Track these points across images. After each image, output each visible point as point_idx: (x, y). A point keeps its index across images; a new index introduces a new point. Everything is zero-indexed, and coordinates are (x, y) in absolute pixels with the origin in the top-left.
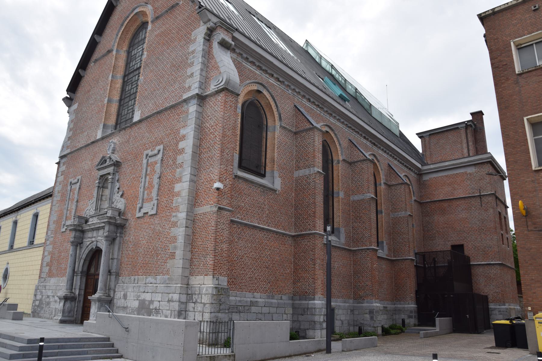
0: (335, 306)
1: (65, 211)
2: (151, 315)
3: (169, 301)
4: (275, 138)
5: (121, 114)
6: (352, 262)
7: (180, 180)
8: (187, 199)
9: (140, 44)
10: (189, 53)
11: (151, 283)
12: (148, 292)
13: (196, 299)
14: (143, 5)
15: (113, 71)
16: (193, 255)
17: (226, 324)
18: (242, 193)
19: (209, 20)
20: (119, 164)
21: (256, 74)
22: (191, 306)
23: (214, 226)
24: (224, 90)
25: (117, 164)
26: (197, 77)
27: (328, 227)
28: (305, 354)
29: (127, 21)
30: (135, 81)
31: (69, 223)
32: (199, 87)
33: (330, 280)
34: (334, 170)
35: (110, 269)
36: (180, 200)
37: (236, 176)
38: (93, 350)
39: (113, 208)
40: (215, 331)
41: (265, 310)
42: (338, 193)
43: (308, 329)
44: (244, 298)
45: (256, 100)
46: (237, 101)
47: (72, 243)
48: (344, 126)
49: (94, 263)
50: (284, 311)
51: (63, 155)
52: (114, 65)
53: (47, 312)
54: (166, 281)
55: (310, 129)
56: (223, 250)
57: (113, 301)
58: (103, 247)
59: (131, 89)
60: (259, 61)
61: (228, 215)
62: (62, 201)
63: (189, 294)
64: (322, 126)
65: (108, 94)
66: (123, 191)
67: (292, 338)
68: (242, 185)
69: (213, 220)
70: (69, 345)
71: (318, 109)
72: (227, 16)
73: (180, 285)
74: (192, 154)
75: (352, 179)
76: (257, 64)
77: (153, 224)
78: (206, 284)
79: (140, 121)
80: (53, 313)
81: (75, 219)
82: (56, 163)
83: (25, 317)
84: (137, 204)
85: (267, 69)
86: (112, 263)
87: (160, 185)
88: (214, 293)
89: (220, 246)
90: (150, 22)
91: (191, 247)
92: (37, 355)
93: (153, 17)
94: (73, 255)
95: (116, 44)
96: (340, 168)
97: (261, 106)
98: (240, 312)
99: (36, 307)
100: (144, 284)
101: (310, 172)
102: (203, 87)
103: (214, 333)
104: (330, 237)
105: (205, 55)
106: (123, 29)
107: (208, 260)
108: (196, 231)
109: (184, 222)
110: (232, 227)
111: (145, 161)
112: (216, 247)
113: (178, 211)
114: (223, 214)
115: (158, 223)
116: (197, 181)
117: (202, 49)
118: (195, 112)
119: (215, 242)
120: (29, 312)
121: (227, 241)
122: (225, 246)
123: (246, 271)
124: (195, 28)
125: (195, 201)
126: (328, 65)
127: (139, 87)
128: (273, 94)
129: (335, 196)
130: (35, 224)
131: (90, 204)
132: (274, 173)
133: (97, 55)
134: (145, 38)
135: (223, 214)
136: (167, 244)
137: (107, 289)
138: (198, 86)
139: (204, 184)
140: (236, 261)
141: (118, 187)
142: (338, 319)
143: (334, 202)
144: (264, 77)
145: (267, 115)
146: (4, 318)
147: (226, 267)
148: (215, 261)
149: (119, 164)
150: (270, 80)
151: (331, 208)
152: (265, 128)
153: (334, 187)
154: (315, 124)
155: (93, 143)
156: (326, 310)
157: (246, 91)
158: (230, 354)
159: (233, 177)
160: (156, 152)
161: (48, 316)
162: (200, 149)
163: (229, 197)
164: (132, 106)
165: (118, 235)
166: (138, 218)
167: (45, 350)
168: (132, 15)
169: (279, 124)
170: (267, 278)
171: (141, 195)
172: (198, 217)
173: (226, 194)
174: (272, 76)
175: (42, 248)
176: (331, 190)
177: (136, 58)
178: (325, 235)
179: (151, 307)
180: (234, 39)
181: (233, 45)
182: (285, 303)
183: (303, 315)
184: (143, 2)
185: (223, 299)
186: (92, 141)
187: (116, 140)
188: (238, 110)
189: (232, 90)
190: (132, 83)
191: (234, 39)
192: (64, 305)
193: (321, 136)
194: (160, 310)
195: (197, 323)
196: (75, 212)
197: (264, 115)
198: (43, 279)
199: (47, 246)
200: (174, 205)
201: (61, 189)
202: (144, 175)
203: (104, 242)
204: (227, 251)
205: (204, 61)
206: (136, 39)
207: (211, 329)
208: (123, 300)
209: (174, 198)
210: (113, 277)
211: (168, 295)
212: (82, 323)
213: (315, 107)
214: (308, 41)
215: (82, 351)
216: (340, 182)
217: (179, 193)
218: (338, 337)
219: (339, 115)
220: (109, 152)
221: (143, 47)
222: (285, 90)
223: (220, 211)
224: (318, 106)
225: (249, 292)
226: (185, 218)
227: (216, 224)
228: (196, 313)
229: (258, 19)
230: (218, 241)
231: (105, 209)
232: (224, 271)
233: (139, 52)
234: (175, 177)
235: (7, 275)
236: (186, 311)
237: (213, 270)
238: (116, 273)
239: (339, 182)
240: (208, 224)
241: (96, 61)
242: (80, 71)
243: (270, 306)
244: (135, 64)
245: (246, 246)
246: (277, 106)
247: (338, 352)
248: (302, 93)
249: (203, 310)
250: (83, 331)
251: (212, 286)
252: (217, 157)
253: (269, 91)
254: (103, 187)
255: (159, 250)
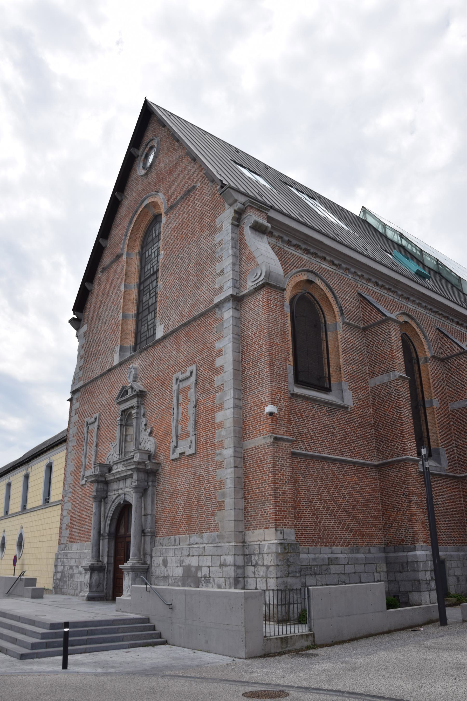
0: (445, 557)
1: (83, 459)
2: (199, 585)
3: (221, 566)
4: (337, 339)
5: (141, 331)
6: (462, 493)
7: (221, 407)
8: (232, 431)
9: (155, 243)
10: (215, 245)
11: (196, 544)
12: (193, 556)
13: (256, 561)
14: (153, 195)
15: (125, 280)
16: (246, 503)
17: (299, 592)
18: (304, 416)
19: (236, 201)
20: (143, 393)
21: (303, 260)
22: (250, 570)
23: (270, 463)
24: (264, 286)
25: (141, 395)
26: (229, 274)
27: (422, 449)
28: (410, 627)
29: (136, 216)
30: (153, 289)
31: (89, 473)
32: (233, 286)
33: (435, 521)
34: (421, 372)
35: (144, 528)
36: (223, 433)
37: (293, 394)
38: (129, 635)
39: (141, 450)
40: (284, 603)
41: (350, 569)
42: (431, 402)
43: (410, 592)
44: (320, 555)
45: (308, 293)
46: (283, 298)
47: (95, 498)
48: (428, 312)
49: (123, 522)
50: (375, 569)
51: (75, 389)
52: (126, 272)
53: (71, 587)
54: (215, 539)
55: (383, 322)
56: (286, 493)
57: (150, 570)
58: (132, 501)
59: (150, 299)
60: (305, 243)
61: (288, 447)
62: (79, 446)
63: (247, 555)
64: (398, 315)
65: (122, 309)
66: (152, 428)
67: (390, 606)
68: (302, 405)
69: (269, 455)
70: (100, 629)
71: (391, 294)
72: (257, 192)
73: (233, 544)
74: (233, 372)
75: (448, 380)
76: (303, 246)
77: (193, 467)
78: (268, 539)
79: (164, 338)
80: (79, 589)
81: (96, 468)
82: (68, 400)
83: (46, 594)
84: (170, 443)
85: (316, 251)
86: (146, 521)
87: (196, 416)
88: (280, 552)
89: (281, 488)
90: (163, 214)
91: (243, 492)
92: (62, 644)
93: (167, 207)
94: (97, 514)
95: (126, 246)
96: (429, 369)
97: (315, 299)
98: (315, 574)
99: (58, 581)
100: (187, 545)
101: (390, 378)
102: (238, 286)
103: (284, 605)
104: (427, 463)
105: (235, 244)
106: (132, 227)
107: (267, 508)
108: (248, 471)
109: (232, 461)
110: (295, 462)
111: (175, 387)
112: (276, 490)
113: (223, 447)
114: (281, 446)
115: (199, 465)
116: (243, 406)
117: (230, 238)
118: (231, 318)
119: (274, 483)
120: (50, 587)
121: (290, 481)
122: (287, 488)
123: (318, 518)
124: (219, 213)
125: (243, 433)
126: (396, 234)
127: (159, 296)
128: (329, 283)
129: (427, 406)
130: (49, 481)
131: (112, 448)
132: (342, 385)
133: (104, 263)
134: (160, 234)
135: (281, 446)
136: (213, 490)
137: (142, 553)
138: (231, 285)
139: (253, 409)
140: (305, 506)
141: (144, 423)
142: (452, 574)
143: (427, 415)
144: (314, 262)
145: (324, 310)
146: (22, 596)
147: (291, 515)
148: (276, 508)
149: (143, 393)
150: (322, 265)
151: (424, 422)
152: (324, 327)
153: (425, 394)
154: (388, 314)
155: (109, 370)
156: (432, 563)
157: (293, 283)
158: (307, 633)
159: (289, 395)
160: (187, 374)
161: (72, 591)
162: (243, 364)
163: (286, 423)
164: (153, 320)
165: (150, 484)
166: (173, 460)
167: (72, 637)
168: (141, 209)
169: (341, 321)
170: (348, 525)
171: (174, 430)
172: (250, 453)
173: (282, 419)
174: (324, 259)
175: (59, 507)
176: (421, 398)
177: (151, 260)
178: (420, 461)
179: (199, 575)
180: (269, 219)
181: (269, 227)
182: (375, 557)
183: (401, 572)
184: (152, 191)
185: (292, 558)
186: (108, 368)
187: (137, 364)
188: (285, 308)
189: (275, 284)
190: (150, 291)
191: (269, 219)
192: (91, 578)
193: (398, 328)
194: (211, 579)
195: (261, 594)
196: (95, 459)
197: (320, 311)
198: (64, 546)
199: (65, 503)
200: (217, 440)
201: (76, 432)
202: (175, 404)
203: (134, 494)
204: (291, 494)
205: (235, 253)
206: (149, 237)
207: (279, 600)
208: (163, 568)
209: (216, 431)
210: (148, 539)
211: (219, 557)
212: (114, 600)
213: (386, 292)
214: (365, 208)
215: (117, 637)
216: (432, 387)
217: (221, 424)
218: (454, 600)
219: (419, 299)
220: (130, 380)
221: (158, 245)
222: (343, 275)
223: (277, 442)
224: (389, 290)
225: (325, 546)
226: (233, 455)
227: (273, 460)
228: (258, 580)
229: (297, 190)
230: (278, 482)
231: (131, 452)
232: (289, 520)
233: (154, 252)
234: (215, 403)
235: (22, 542)
236: (244, 577)
237: (275, 520)
238: (151, 533)
239: (430, 387)
240: (263, 460)
241: (104, 269)
242: (86, 284)
243: (355, 562)
244: (151, 268)
245: (315, 485)
246: (335, 297)
247: (457, 623)
248: (366, 276)
249: (267, 575)
250: (116, 611)
251: (276, 541)
252: (265, 373)
253: (322, 279)
254: (126, 425)
255: (204, 500)
